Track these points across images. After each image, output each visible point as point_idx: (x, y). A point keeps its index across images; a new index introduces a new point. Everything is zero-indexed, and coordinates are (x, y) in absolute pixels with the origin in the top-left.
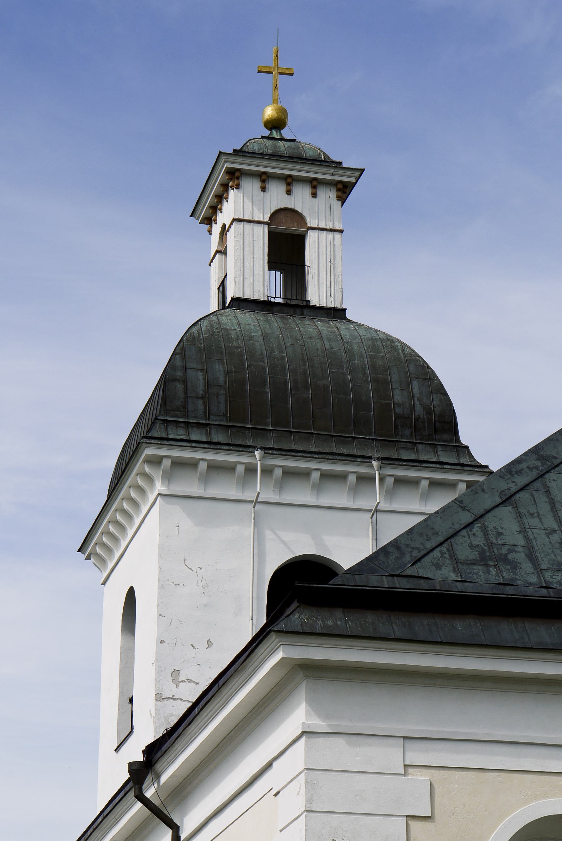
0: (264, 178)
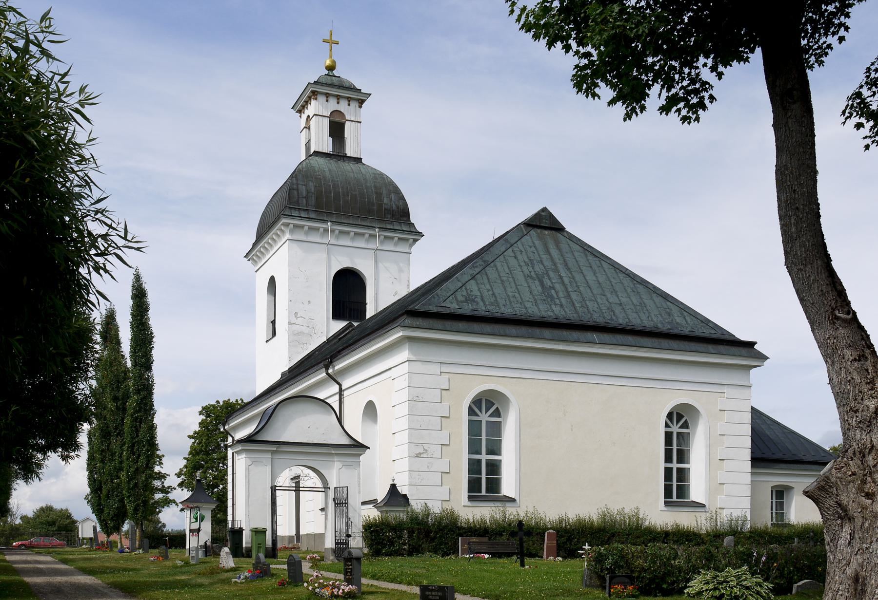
0: (327, 95)
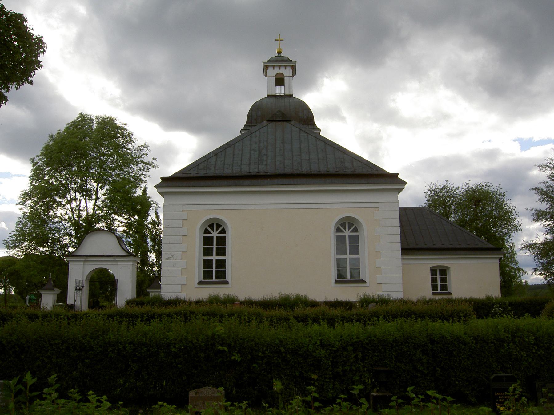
0: (274, 66)
